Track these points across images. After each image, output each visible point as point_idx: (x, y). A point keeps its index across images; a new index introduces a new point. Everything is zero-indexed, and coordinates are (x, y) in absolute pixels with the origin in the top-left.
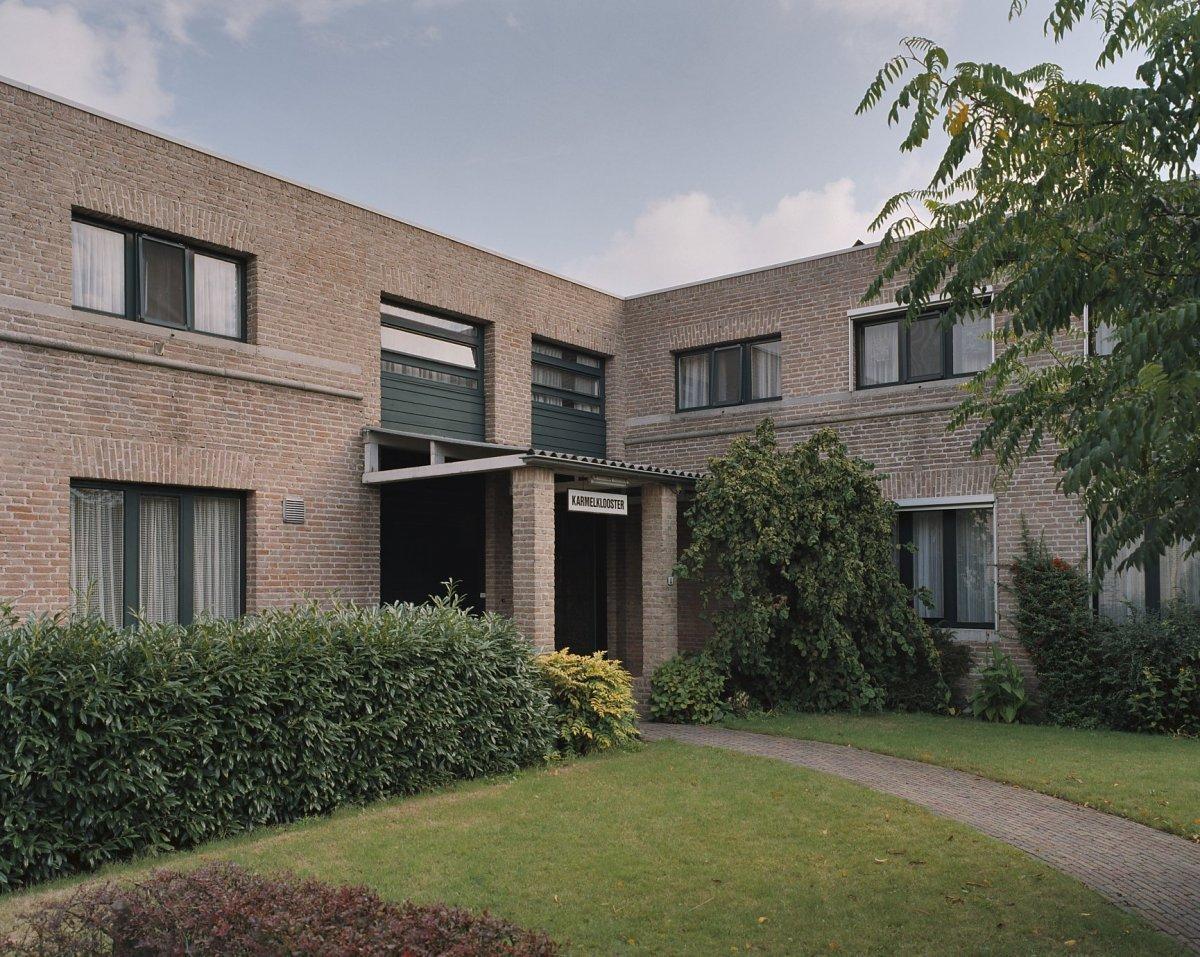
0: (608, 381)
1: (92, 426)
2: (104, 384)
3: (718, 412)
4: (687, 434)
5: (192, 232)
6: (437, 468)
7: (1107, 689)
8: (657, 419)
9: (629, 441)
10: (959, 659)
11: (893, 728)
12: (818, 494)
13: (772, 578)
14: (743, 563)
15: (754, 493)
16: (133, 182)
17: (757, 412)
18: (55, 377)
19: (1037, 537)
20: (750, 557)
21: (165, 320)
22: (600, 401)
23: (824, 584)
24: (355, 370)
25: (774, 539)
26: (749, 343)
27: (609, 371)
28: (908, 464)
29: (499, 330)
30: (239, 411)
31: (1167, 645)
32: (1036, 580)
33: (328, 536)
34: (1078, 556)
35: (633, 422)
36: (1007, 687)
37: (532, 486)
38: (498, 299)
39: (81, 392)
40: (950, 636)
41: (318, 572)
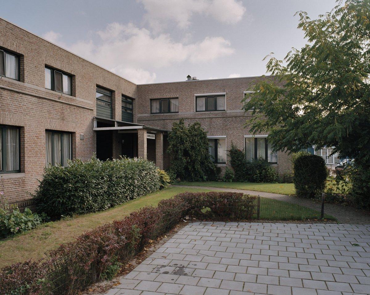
0: (134, 105)
1: (49, 117)
2: (50, 107)
3: (163, 114)
4: (155, 119)
5: (65, 70)
6: (116, 128)
7: (249, 175)
8: (146, 115)
9: (139, 120)
10: (219, 170)
11: (209, 183)
12: (196, 135)
13: (186, 153)
14: (181, 150)
15: (184, 135)
16: (55, 58)
17: (172, 115)
18: (43, 105)
19: (234, 145)
20: (182, 149)
21: (58, 91)
22: (132, 110)
23: (196, 154)
24: (92, 103)
25: (188, 145)
26: (169, 99)
27: (134, 102)
28: (208, 129)
29: (116, 93)
30: (73, 113)
31: (260, 166)
32: (235, 154)
33: (88, 143)
34: (242, 149)
35: (139, 115)
36: (231, 175)
37: (144, 133)
38: (116, 85)
39: (47, 109)
40: (217, 165)
41: (86, 152)
